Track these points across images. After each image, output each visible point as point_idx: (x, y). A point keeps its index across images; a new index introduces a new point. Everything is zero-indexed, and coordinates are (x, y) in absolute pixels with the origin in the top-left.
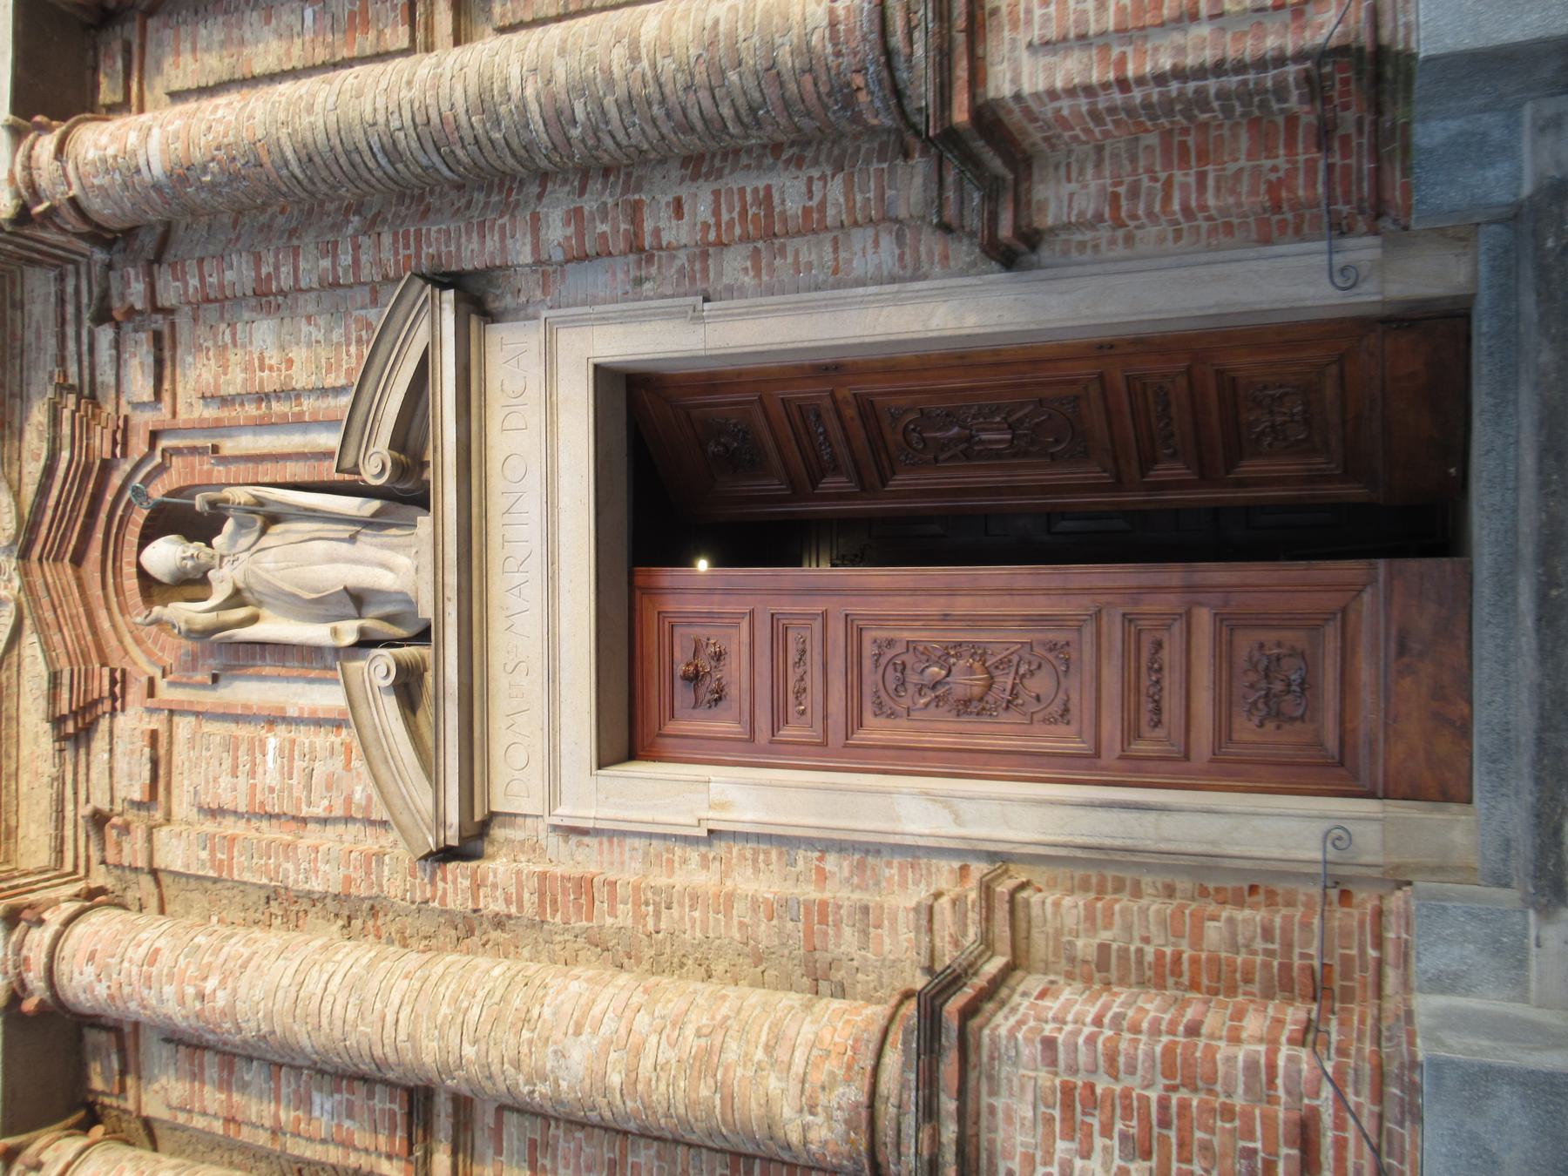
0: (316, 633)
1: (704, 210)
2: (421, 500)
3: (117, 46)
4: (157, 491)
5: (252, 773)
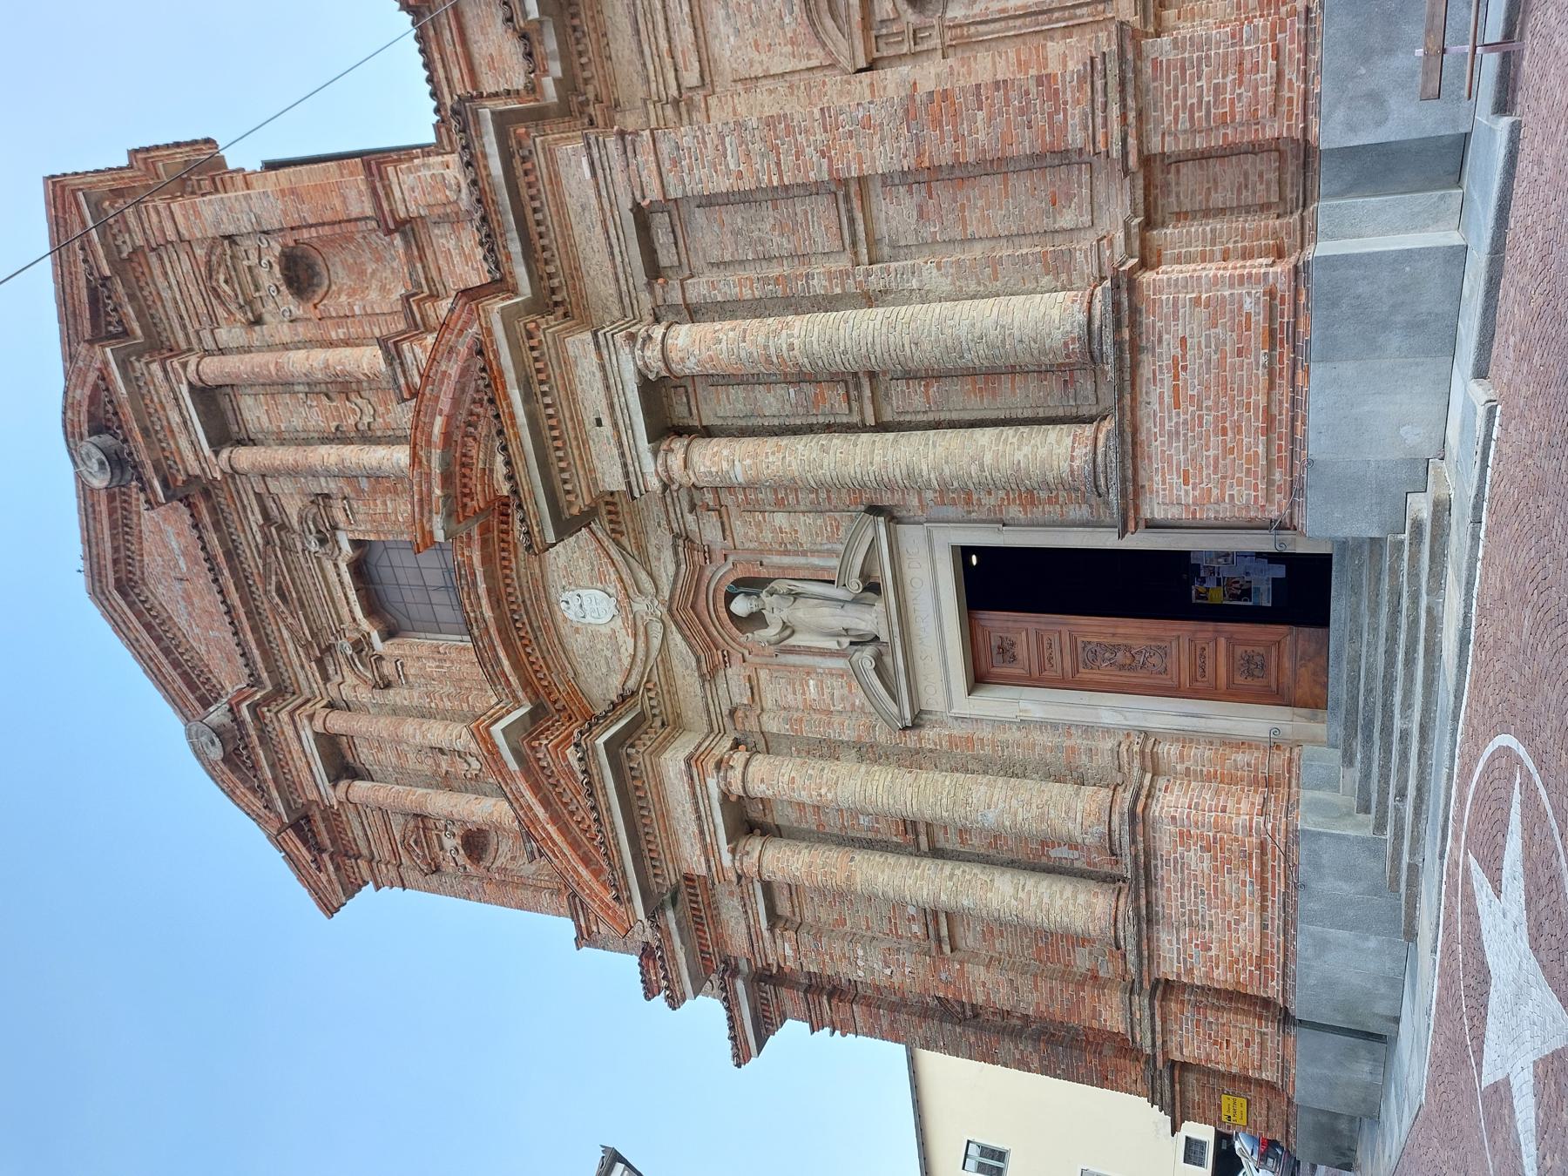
0: (831, 644)
5: (804, 693)
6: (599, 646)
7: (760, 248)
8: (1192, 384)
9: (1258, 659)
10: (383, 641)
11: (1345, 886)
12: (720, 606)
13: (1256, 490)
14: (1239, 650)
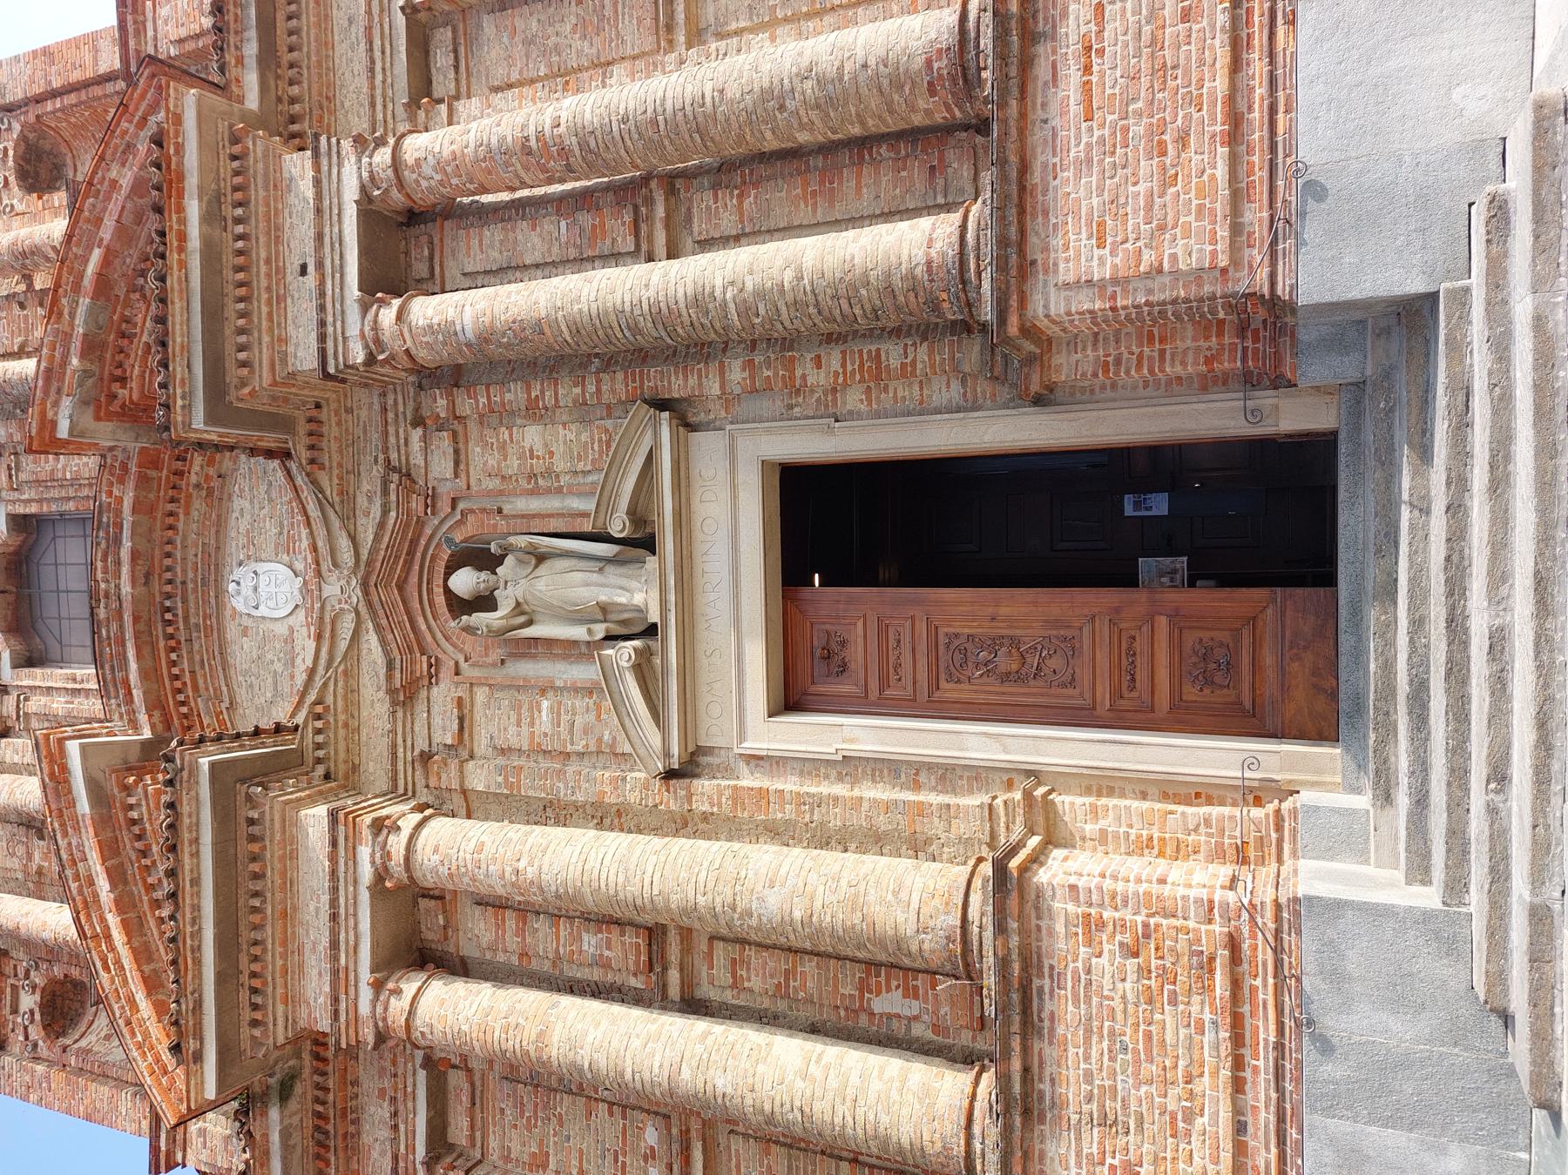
0: (578, 632)
1: (835, 364)
2: (648, 544)
3: (424, 239)
4: (458, 537)
5: (532, 724)
6: (269, 656)
7: (555, 59)
8: (1109, 74)
9: (1219, 654)
10: (15, 666)
11: (1395, 1024)
12: (427, 578)
13: (1213, 241)
14: (1190, 638)
